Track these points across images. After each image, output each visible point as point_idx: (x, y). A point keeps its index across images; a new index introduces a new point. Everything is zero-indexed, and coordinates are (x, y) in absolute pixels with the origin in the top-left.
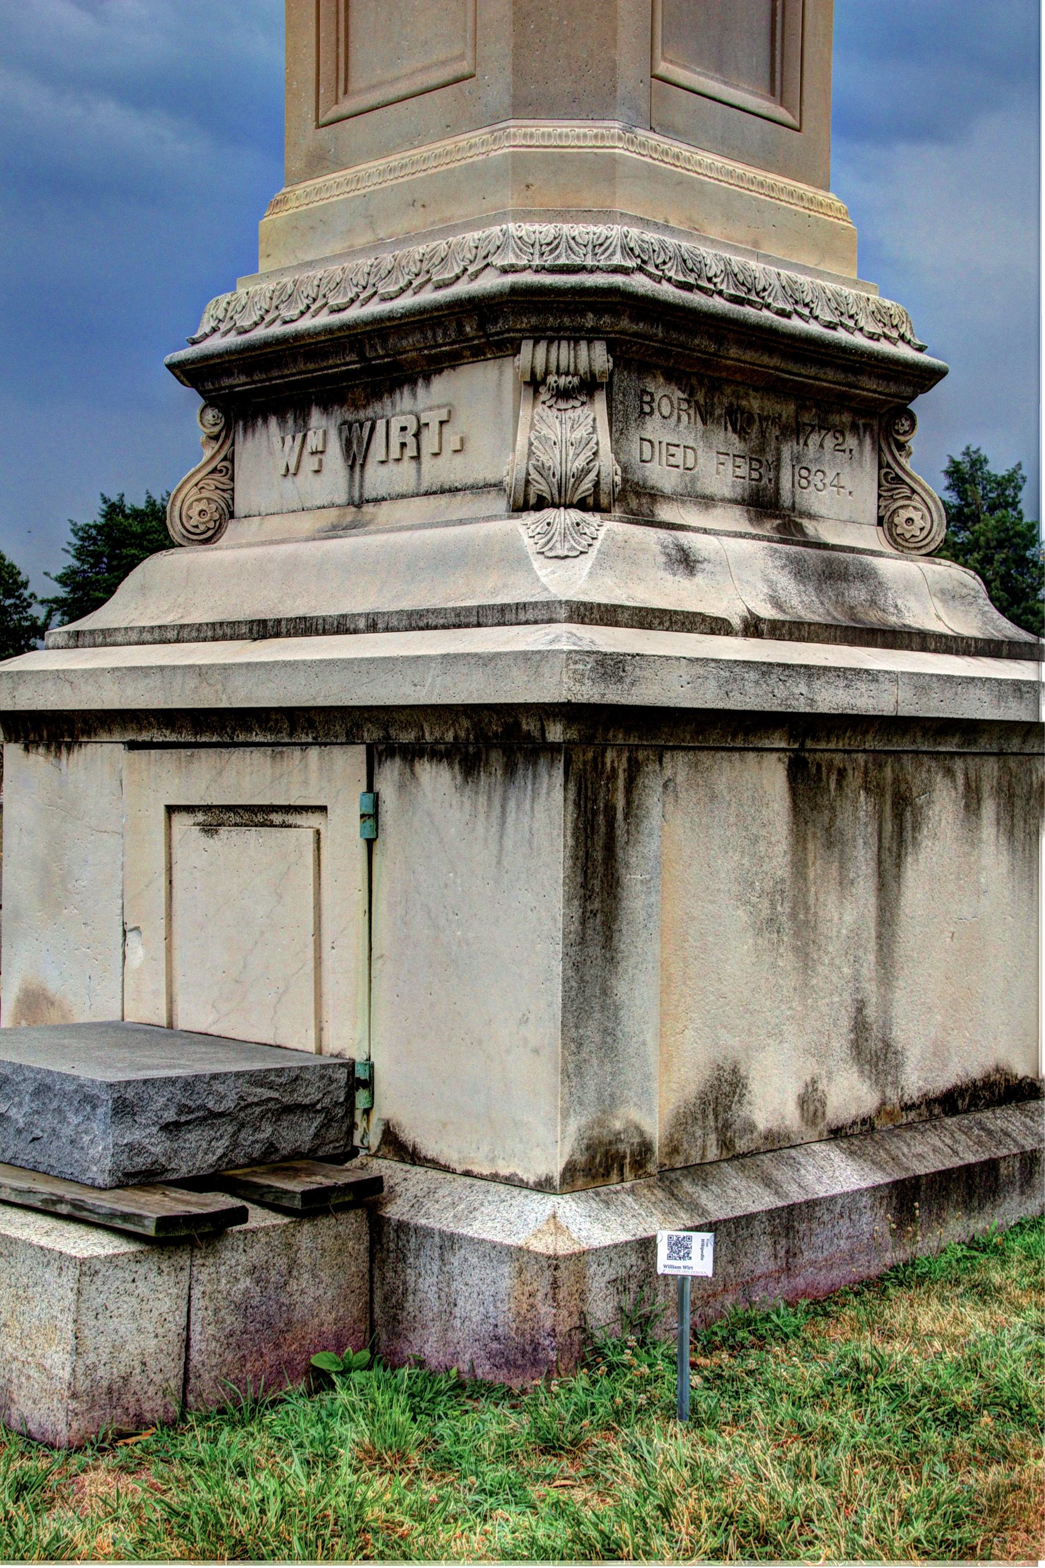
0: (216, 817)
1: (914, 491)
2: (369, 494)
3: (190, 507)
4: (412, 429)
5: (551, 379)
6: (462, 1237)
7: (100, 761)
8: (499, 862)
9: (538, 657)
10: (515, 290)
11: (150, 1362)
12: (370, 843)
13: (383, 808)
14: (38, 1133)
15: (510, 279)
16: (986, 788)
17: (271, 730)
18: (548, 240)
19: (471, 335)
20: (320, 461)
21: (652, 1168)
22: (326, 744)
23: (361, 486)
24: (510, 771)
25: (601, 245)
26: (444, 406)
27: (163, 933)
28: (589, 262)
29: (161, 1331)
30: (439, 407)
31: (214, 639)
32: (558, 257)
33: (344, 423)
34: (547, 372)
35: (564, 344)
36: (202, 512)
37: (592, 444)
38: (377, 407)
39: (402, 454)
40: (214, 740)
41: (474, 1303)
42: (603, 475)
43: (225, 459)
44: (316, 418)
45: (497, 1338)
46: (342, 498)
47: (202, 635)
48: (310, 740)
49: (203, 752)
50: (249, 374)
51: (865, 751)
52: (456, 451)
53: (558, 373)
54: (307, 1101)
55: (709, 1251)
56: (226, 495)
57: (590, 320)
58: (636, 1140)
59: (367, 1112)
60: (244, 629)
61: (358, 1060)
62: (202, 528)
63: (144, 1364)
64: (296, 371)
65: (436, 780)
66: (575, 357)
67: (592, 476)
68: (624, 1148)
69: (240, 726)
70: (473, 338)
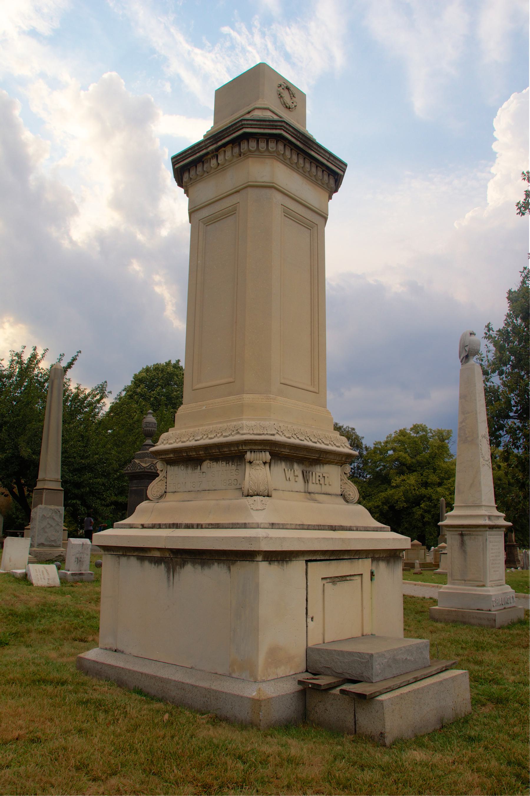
0: (335, 580)
2: (310, 491)
7: (297, 567)
24: (394, 562)
31: (319, 530)
44: (296, 466)
46: (303, 490)
50: (290, 450)
60: (327, 528)
64: (301, 454)
65: (382, 565)
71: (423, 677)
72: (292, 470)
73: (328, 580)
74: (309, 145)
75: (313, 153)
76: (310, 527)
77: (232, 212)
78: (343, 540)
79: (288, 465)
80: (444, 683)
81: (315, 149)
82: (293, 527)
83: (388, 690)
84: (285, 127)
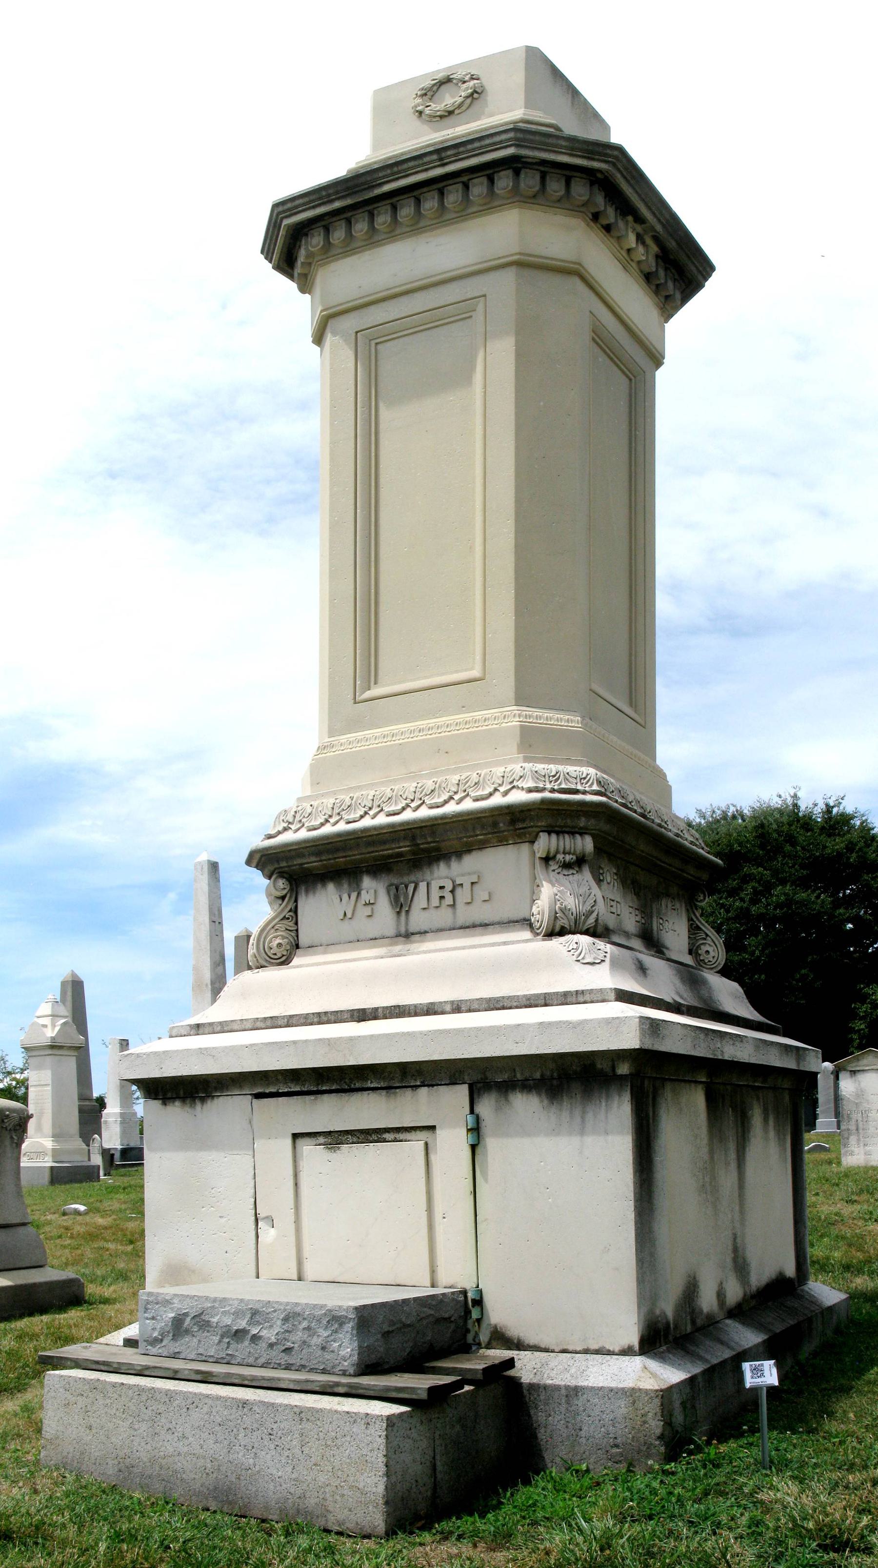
0: (335, 1139)
1: (707, 935)
2: (412, 929)
3: (271, 941)
4: (449, 887)
5: (560, 857)
6: (583, 1388)
8: (581, 1153)
9: (617, 1021)
10: (543, 801)
11: (419, 1480)
12: (473, 1148)
13: (483, 1124)
14: (289, 1344)
15: (537, 796)
16: (770, 1108)
17: (384, 1079)
18: (553, 774)
19: (503, 829)
20: (372, 909)
21: (671, 1338)
22: (433, 1086)
23: (407, 924)
25: (585, 778)
26: (474, 873)
27: (293, 1218)
28: (579, 787)
29: (423, 1460)
30: (469, 874)
31: (320, 1023)
32: (560, 784)
33: (391, 885)
34: (557, 852)
35: (567, 836)
36: (279, 945)
37: (592, 895)
38: (419, 875)
39: (440, 903)
40: (334, 1088)
41: (596, 1427)
42: (600, 915)
43: (290, 911)
44: (367, 882)
45: (617, 1446)
47: (309, 1021)
48: (418, 1083)
49: (326, 1097)
51: (731, 1084)
52: (485, 901)
53: (564, 853)
54: (447, 1315)
55: (774, 1371)
56: (293, 934)
57: (582, 822)
58: (664, 1321)
59: (479, 1321)
61: (468, 1288)
62: (279, 955)
63: (417, 1481)
65: (526, 1106)
66: (575, 844)
67: (594, 915)
68: (660, 1326)
69: (357, 1077)
70: (504, 831)
71: (236, 1381)
72: (354, 895)
73: (321, 1140)
74: (362, 184)
75: (378, 191)
76: (294, 1021)
77: (471, 317)
78: (329, 1043)
79: (346, 886)
80: (255, 1408)
81: (384, 177)
82: (249, 1026)
83: (103, 1368)
84: (284, 212)
